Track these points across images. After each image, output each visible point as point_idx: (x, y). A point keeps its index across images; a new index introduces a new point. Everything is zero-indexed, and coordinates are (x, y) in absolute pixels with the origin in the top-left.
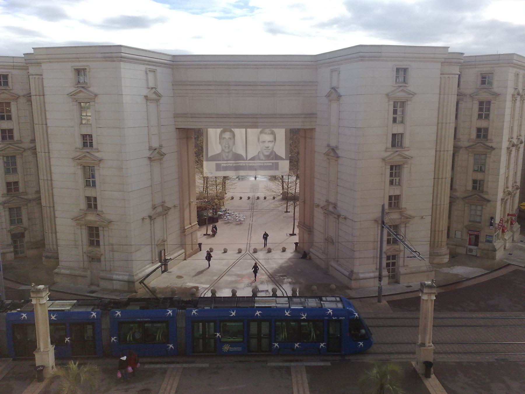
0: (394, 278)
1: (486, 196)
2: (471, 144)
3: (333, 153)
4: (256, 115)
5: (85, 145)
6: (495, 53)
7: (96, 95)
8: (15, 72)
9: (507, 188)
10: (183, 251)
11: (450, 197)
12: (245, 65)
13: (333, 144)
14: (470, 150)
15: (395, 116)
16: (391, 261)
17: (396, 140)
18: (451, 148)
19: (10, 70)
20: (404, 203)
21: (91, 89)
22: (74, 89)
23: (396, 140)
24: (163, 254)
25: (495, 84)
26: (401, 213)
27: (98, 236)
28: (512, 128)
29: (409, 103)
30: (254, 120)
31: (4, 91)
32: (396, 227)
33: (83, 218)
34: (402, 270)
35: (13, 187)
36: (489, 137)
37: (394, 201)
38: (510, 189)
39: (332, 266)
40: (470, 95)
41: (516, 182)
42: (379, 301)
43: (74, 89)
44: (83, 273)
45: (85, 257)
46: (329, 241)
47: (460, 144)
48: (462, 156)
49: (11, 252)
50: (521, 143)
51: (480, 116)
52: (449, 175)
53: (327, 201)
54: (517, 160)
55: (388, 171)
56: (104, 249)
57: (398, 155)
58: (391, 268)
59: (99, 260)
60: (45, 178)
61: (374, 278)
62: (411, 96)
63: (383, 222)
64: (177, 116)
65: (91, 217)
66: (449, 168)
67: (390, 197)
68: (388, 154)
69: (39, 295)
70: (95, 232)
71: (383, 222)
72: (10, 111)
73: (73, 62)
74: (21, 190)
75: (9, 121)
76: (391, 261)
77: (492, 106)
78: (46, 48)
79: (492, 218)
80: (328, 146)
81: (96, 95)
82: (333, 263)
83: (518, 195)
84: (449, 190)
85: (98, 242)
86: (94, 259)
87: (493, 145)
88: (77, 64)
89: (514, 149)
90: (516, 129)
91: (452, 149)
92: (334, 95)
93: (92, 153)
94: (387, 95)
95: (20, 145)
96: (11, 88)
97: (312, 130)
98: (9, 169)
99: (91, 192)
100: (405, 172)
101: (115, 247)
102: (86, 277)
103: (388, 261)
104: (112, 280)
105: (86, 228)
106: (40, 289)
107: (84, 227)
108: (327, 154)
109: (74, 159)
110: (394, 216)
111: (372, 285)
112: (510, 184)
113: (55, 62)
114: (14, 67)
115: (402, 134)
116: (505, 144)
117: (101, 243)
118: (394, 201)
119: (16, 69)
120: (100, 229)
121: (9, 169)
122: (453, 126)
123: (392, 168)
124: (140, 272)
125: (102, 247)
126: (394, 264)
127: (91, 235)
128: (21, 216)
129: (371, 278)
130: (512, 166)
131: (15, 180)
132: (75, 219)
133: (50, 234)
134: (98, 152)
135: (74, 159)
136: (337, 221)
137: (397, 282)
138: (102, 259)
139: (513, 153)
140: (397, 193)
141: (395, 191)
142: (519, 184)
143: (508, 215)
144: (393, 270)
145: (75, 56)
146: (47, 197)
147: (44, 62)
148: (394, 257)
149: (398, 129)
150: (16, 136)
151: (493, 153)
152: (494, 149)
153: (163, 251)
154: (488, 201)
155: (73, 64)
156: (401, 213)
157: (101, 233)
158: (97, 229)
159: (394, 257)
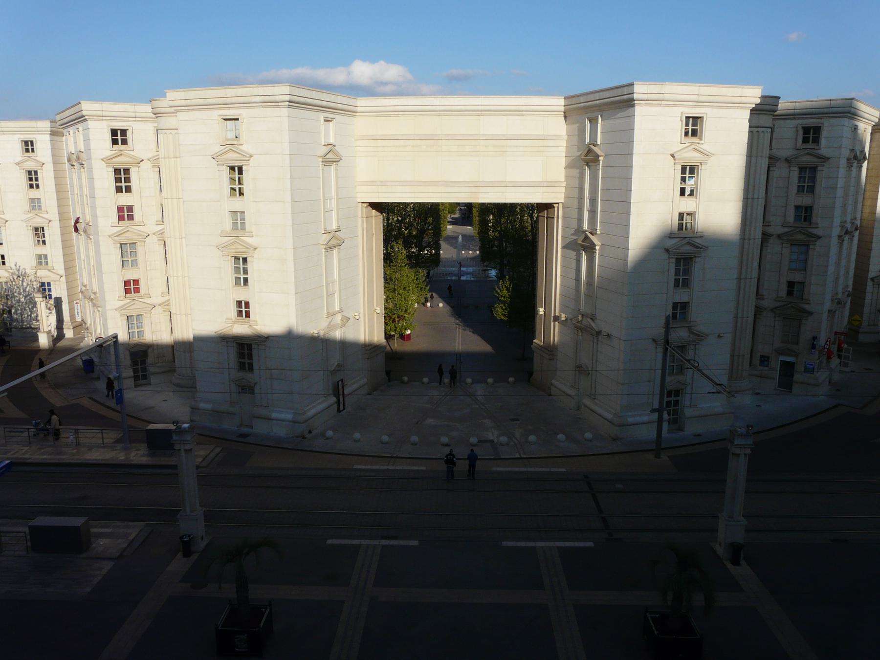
0: (677, 422)
1: (806, 307)
6: (636, 127)
9: (837, 294)
11: (756, 307)
14: (785, 238)
15: (683, 186)
16: (673, 399)
18: (759, 236)
20: (696, 314)
21: (244, 148)
25: (823, 142)
26: (690, 329)
27: (250, 356)
28: (844, 206)
32: (683, 348)
34: (688, 412)
35: (132, 287)
36: (814, 219)
37: (680, 310)
38: (839, 296)
39: (585, 406)
40: (786, 160)
41: (847, 286)
42: (658, 456)
47: (770, 230)
48: (774, 246)
50: (856, 229)
51: (800, 189)
52: (755, 275)
54: (849, 255)
55: (673, 267)
57: (689, 243)
58: (672, 408)
61: (649, 422)
63: (667, 342)
66: (756, 264)
67: (675, 305)
71: (667, 342)
76: (673, 399)
77: (819, 174)
79: (815, 338)
82: (587, 401)
83: (848, 305)
84: (755, 295)
85: (251, 365)
86: (247, 389)
88: (22, 136)
89: (846, 238)
90: (850, 208)
91: (760, 236)
99: (242, 294)
100: (697, 268)
102: (234, 414)
103: (676, 398)
104: (270, 419)
106: (185, 429)
110: (680, 334)
111: (648, 433)
112: (840, 290)
116: (836, 231)
117: (255, 366)
118: (680, 310)
122: (762, 202)
123: (678, 260)
126: (676, 403)
127: (241, 355)
128: (142, 327)
129: (643, 423)
130: (844, 262)
136: (595, 340)
137: (681, 429)
138: (257, 391)
139: (845, 243)
140: (685, 299)
141: (682, 296)
142: (850, 289)
143: (836, 333)
144: (676, 412)
147: (90, 120)
148: (677, 393)
152: (819, 237)
154: (810, 313)
155: (110, 123)
156: (690, 329)
157: (254, 352)
159: (677, 393)
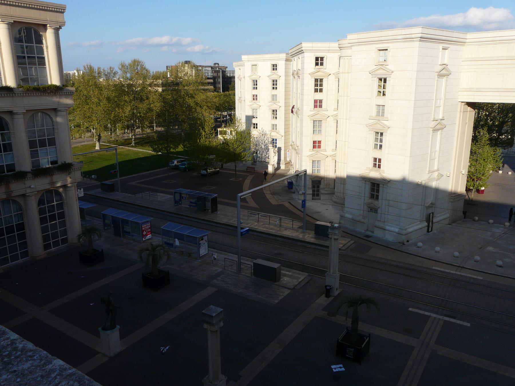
5: (273, 99)
24: (431, 217)
27: (378, 191)
44: (363, 220)
45: (366, 207)
56: (381, 203)
59: (376, 211)
70: (376, 188)
86: (373, 210)
98: (377, 144)
101: (391, 202)
105: (370, 183)
115: (320, 199)
117: (380, 197)
120: (380, 185)
121: (377, 144)
124: (409, 228)
125: (380, 200)
127: (373, 190)
138: (379, 211)
153: (431, 214)
157: (381, 189)
158: (378, 185)
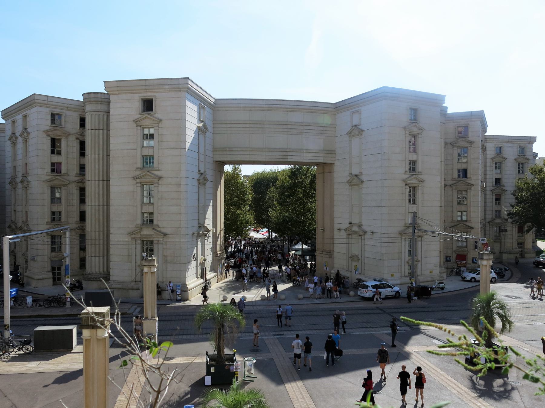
2: (454, 182)
3: (356, 180)
4: (287, 149)
7: (160, 120)
8: (68, 113)
10: (215, 274)
12: (277, 108)
13: (355, 172)
14: (454, 187)
17: (413, 166)
19: (64, 111)
22: (139, 116)
23: (413, 166)
29: (420, 136)
30: (284, 153)
31: (58, 128)
33: (138, 233)
43: (139, 116)
46: (353, 258)
49: (50, 278)
53: (350, 223)
60: (93, 204)
62: (421, 131)
64: (215, 150)
65: (147, 231)
68: (407, 176)
69: (151, 264)
72: (60, 147)
73: (141, 93)
74: (63, 219)
75: (59, 156)
78: (117, 81)
80: (351, 175)
81: (160, 120)
87: (472, 182)
88: (144, 95)
92: (356, 131)
93: (153, 172)
94: (404, 128)
95: (65, 177)
96: (63, 126)
97: (331, 164)
107: (139, 241)
108: (349, 182)
109: (134, 178)
113: (123, 93)
114: (68, 109)
119: (69, 110)
120: (155, 242)
131: (59, 210)
132: (131, 234)
133: (93, 258)
134: (159, 170)
135: (134, 178)
145: (144, 88)
146: (93, 221)
149: (413, 157)
150: (64, 170)
151: (473, 188)
155: (141, 95)
